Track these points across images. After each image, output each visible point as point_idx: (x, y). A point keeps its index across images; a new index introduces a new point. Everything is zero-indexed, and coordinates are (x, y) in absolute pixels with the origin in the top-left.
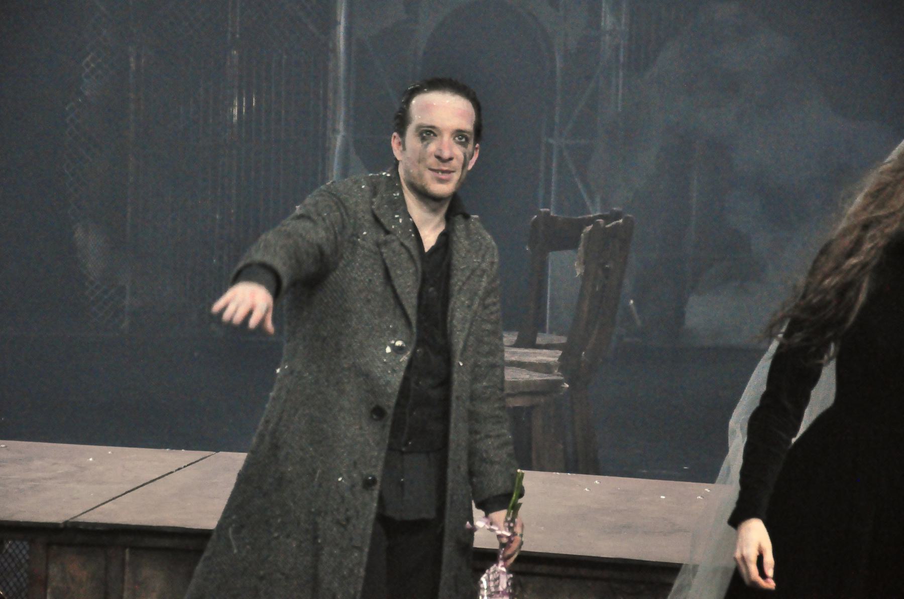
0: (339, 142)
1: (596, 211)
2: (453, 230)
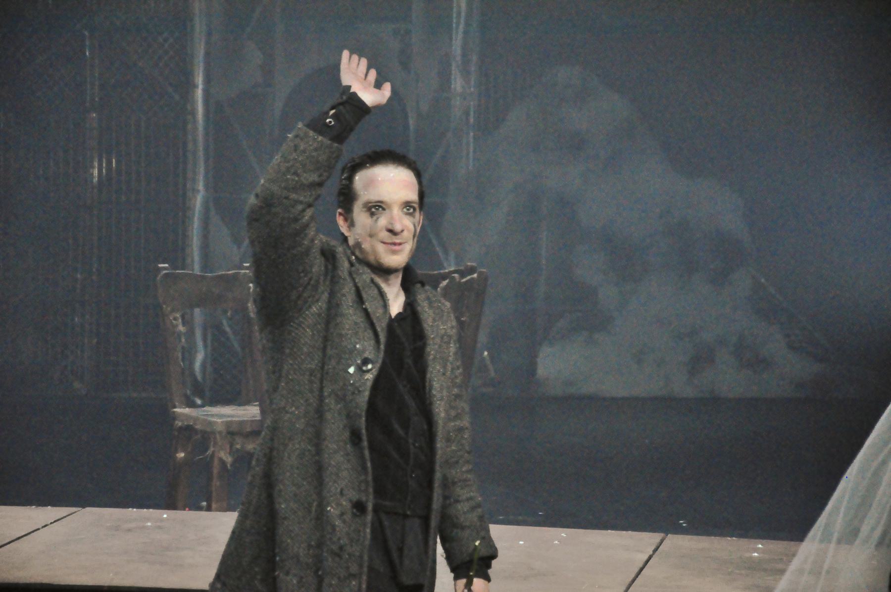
0: (198, 201)
1: (450, 265)
2: (415, 300)
